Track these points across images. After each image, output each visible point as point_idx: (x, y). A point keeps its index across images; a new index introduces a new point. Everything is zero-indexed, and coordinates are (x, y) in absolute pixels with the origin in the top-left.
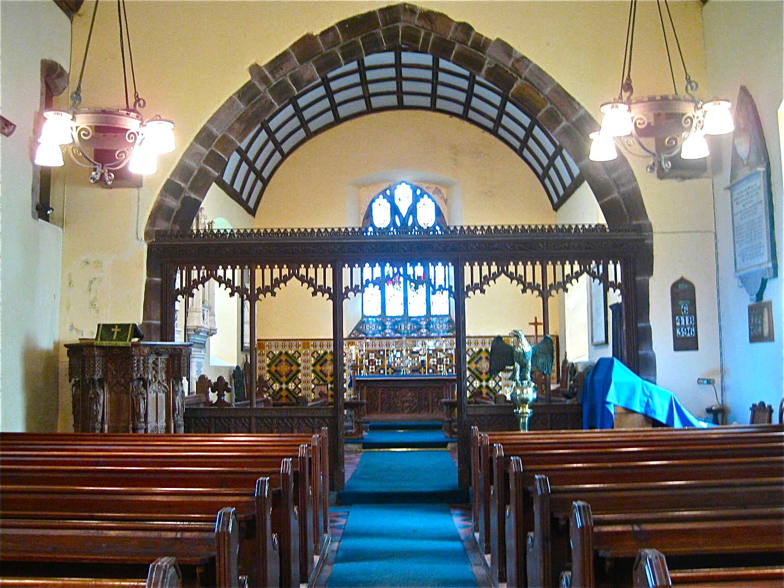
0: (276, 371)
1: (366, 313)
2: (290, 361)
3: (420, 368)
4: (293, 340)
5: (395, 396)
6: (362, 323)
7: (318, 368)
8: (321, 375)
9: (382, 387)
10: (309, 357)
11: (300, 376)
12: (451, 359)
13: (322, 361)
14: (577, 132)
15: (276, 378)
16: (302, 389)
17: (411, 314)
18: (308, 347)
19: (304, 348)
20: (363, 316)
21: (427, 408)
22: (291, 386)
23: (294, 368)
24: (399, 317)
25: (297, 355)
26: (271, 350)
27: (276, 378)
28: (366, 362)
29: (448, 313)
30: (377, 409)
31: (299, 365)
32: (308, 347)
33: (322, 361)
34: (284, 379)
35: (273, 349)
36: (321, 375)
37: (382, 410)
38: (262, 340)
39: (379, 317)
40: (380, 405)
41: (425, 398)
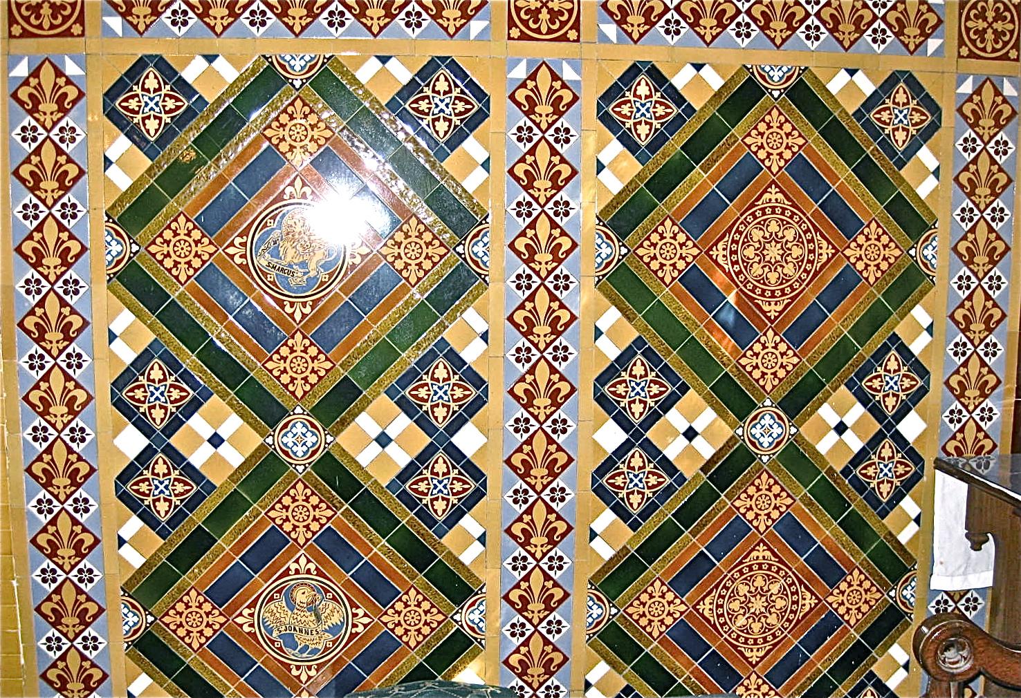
16: (495, 472)
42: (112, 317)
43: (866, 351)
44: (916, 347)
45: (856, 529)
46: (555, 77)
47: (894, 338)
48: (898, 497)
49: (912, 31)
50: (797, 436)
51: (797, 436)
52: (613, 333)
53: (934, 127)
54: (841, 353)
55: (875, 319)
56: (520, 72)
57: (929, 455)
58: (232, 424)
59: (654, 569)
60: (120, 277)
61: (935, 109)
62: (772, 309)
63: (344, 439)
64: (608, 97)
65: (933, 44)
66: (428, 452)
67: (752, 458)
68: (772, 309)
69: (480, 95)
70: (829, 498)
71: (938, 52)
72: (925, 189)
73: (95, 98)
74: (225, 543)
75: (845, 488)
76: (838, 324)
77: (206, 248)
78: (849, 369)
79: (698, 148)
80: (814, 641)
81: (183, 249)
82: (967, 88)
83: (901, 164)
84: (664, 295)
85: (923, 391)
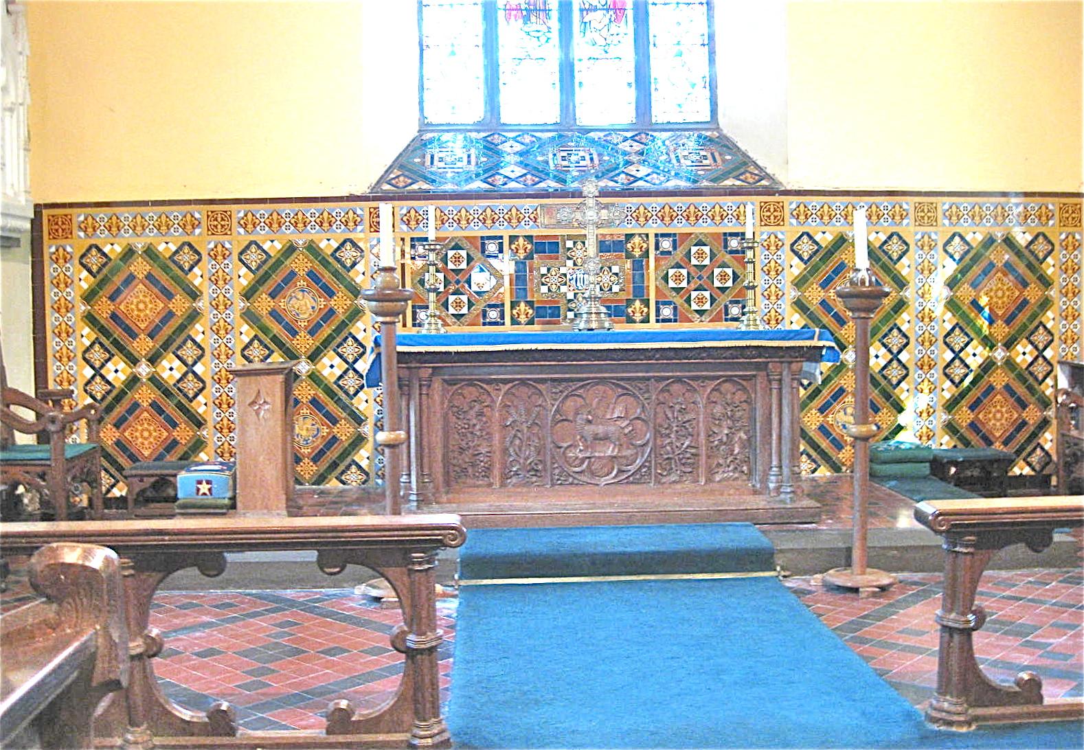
0: (114, 317)
1: (432, 118)
2: (164, 279)
3: (629, 302)
4: (144, 203)
5: (561, 418)
6: (419, 145)
7: (264, 303)
8: (276, 329)
9: (505, 382)
10: (233, 264)
11: (198, 331)
12: (661, 283)
13: (277, 278)
14: (890, 674)
15: (116, 343)
16: (209, 381)
17: (586, 116)
18: (933, 222)
19: (212, 230)
20: (425, 126)
21: (688, 464)
22: (170, 369)
23: (180, 304)
24: (544, 128)
25: (186, 258)
26: (352, 236)
27: (116, 343)
28: (434, 279)
29: (706, 117)
30: (488, 470)
31: (194, 294)
32: (933, 222)
33: (277, 278)
34: (142, 345)
35: (101, 238)
36: (276, 329)
37: (505, 477)
38: (63, 206)
39: (479, 126)
40: (497, 456)
41: (682, 425)
42: (241, 326)
43: (1032, 327)
44: (1049, 326)
45: (1031, 389)
46: (930, 237)
47: (1041, 323)
48: (1045, 378)
49: (1044, 218)
50: (1010, 356)
51: (1010, 356)
52: (88, 337)
53: (1052, 250)
54: (1024, 327)
55: (1034, 317)
56: (212, 245)
57: (1054, 362)
58: (122, 366)
59: (963, 402)
60: (86, 317)
61: (1053, 245)
62: (1000, 313)
63: (1013, 354)
64: (241, 253)
65: (1051, 222)
66: (891, 361)
67: (994, 363)
68: (1000, 313)
69: (907, 244)
70: (1021, 378)
71: (1053, 225)
72: (1050, 271)
73: (235, 256)
74: (825, 392)
75: (1026, 374)
76: (1022, 318)
77: (822, 294)
78: (1027, 333)
79: (975, 260)
80: (1018, 429)
81: (264, 304)
82: (1063, 237)
83: (1041, 263)
84: (965, 308)
85: (1052, 341)
